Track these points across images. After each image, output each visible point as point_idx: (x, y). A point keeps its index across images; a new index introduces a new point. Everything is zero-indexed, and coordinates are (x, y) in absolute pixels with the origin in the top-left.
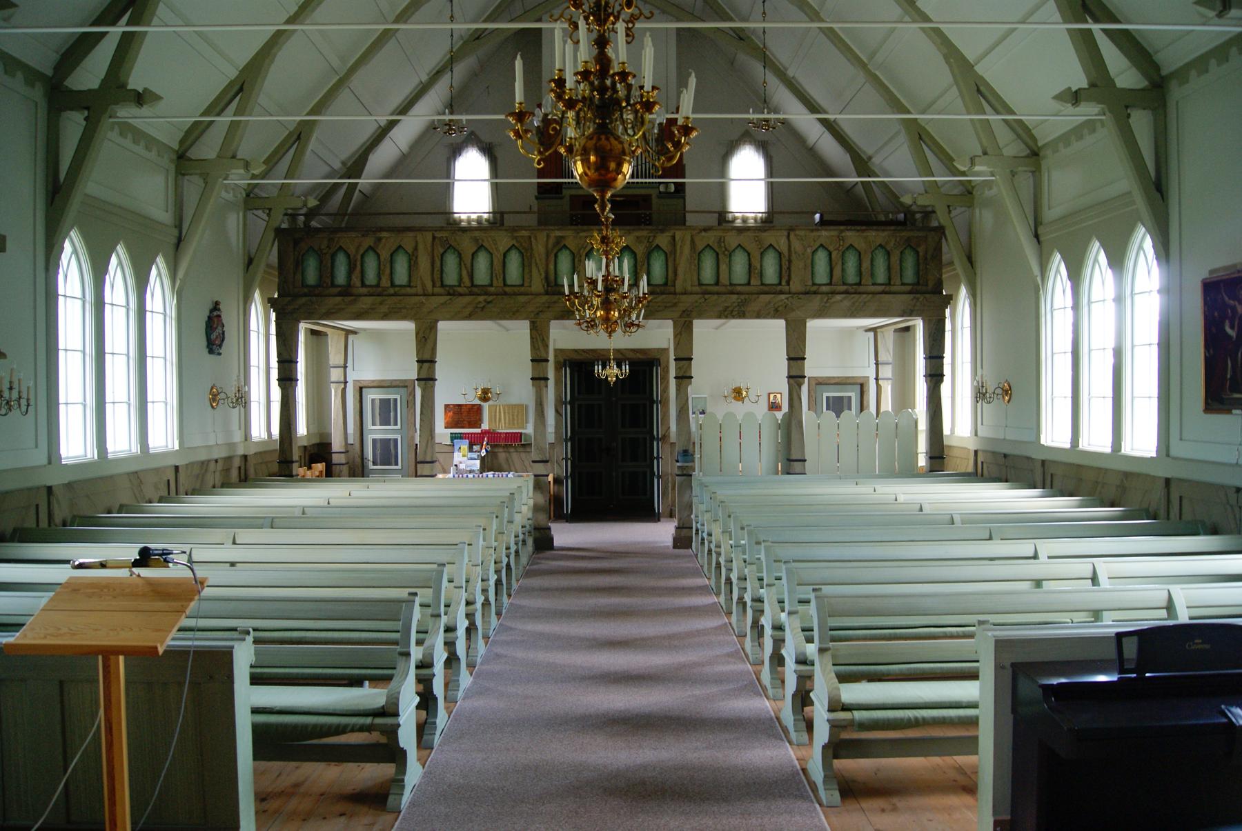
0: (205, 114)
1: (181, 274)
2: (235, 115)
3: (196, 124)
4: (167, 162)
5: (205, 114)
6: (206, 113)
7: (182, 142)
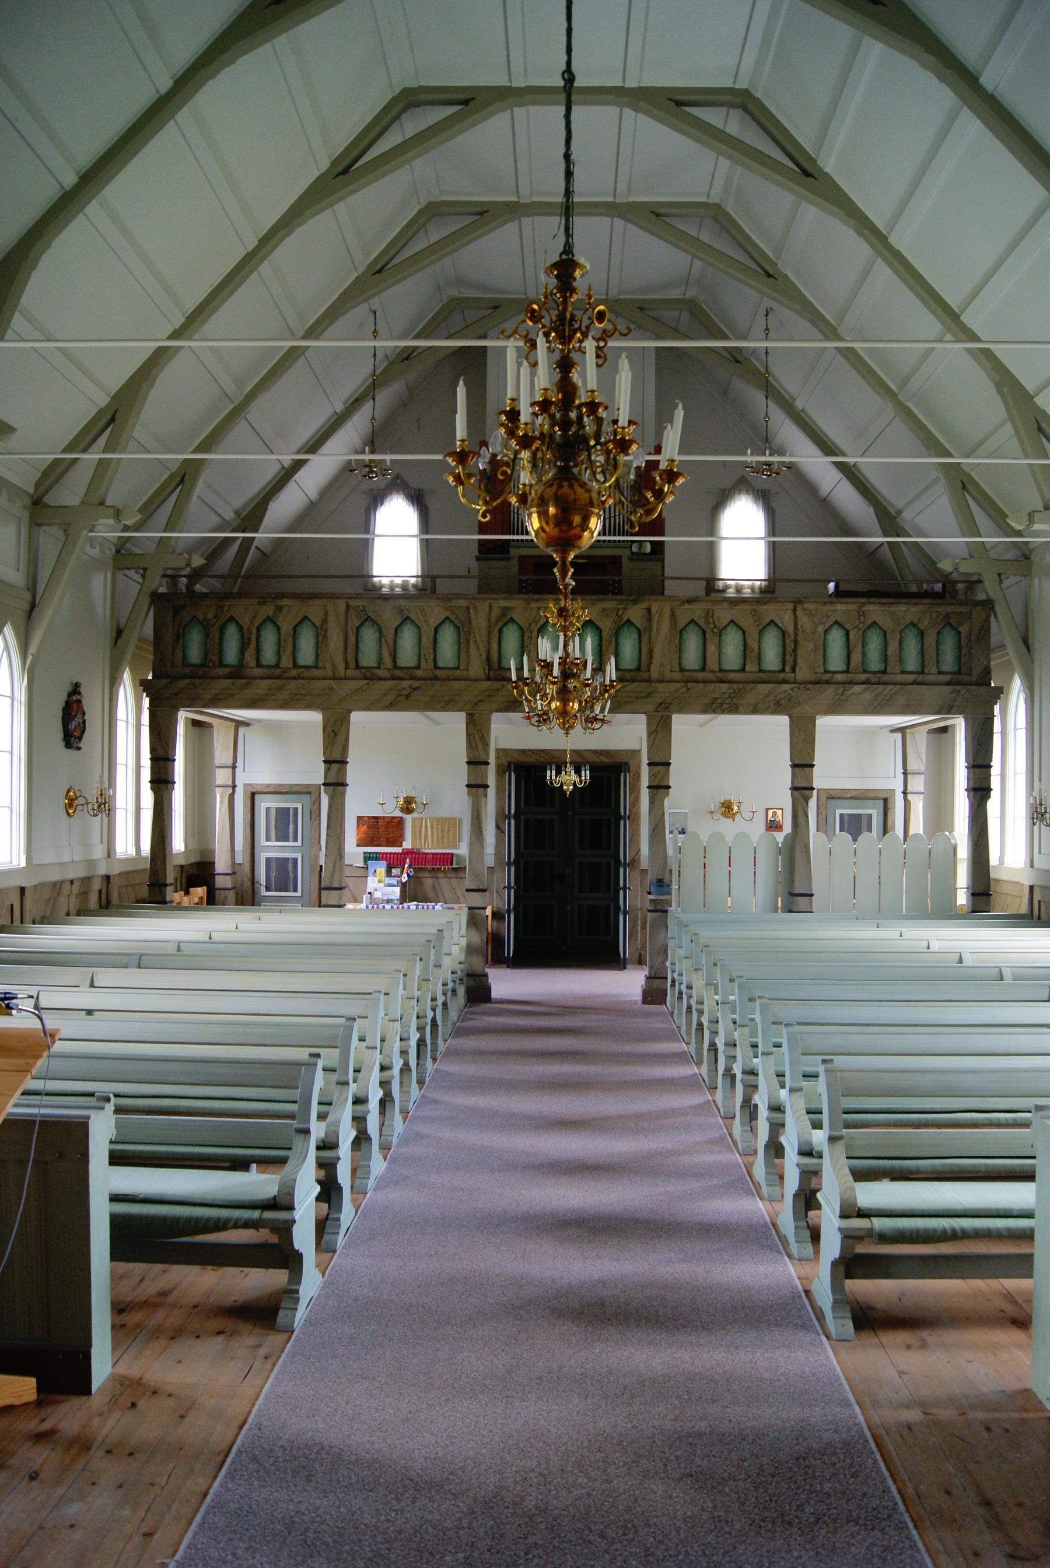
0: (65, 450)
1: (33, 648)
2: (104, 452)
3: (56, 462)
4: (19, 509)
5: (65, 450)
6: (68, 449)
7: (38, 484)
